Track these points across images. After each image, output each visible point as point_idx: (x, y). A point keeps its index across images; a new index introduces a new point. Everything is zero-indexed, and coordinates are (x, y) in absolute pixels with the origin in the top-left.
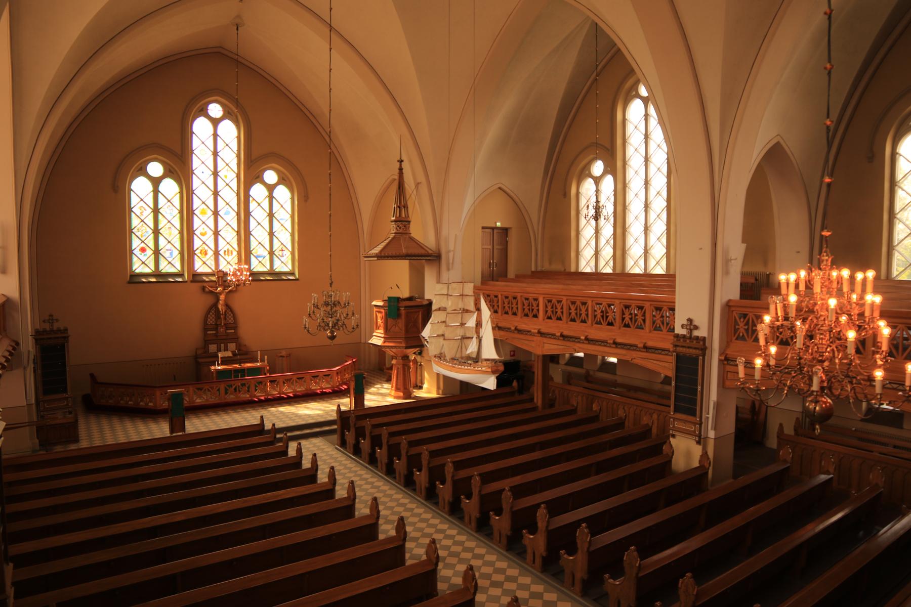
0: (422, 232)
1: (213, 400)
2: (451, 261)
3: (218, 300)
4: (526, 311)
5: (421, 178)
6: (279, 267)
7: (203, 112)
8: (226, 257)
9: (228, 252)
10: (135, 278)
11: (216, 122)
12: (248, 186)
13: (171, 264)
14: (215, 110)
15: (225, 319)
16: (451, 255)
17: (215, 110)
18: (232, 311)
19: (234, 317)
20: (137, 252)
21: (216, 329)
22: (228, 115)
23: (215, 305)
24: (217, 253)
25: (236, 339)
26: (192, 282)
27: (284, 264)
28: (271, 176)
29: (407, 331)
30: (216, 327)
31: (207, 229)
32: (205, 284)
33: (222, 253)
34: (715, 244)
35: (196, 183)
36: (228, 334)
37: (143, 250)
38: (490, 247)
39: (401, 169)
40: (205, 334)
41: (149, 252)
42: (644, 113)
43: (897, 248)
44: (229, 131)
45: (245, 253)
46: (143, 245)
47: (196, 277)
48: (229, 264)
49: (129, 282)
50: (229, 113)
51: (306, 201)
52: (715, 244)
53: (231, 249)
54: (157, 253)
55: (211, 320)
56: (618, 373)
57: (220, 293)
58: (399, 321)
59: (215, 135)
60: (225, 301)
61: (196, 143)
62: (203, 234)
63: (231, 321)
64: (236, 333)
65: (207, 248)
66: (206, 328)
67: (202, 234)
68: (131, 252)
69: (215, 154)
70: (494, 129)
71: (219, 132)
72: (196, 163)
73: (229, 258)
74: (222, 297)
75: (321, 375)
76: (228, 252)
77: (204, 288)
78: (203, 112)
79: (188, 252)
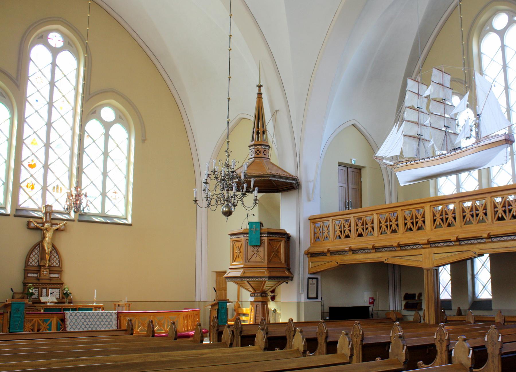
0: (283, 160)
2: (311, 191)
3: (44, 237)
4: (409, 225)
5: (280, 105)
6: (111, 211)
7: (43, 39)
8: (55, 194)
9: (56, 188)
11: (55, 52)
12: (84, 121)
14: (56, 39)
15: (50, 261)
17: (56, 39)
18: (57, 253)
19: (60, 260)
21: (39, 272)
22: (68, 45)
23: (40, 244)
24: (45, 189)
25: (59, 285)
27: (119, 207)
28: (108, 114)
29: (269, 261)
30: (39, 268)
32: (32, 220)
33: (50, 188)
35: (28, 110)
36: (51, 279)
38: (346, 185)
39: (260, 94)
40: (25, 277)
42: (500, 44)
44: (69, 63)
47: (19, 213)
48: (59, 203)
50: (69, 44)
51: (144, 141)
53: (60, 185)
55: (34, 261)
56: (493, 308)
58: (261, 249)
59: (54, 65)
61: (32, 69)
63: (56, 263)
64: (59, 278)
65: (34, 182)
66: (27, 270)
67: (30, 165)
69: (52, 84)
70: (354, 57)
71: (57, 62)
72: (30, 89)
74: (49, 235)
76: (56, 188)
77: (29, 223)
78: (43, 39)
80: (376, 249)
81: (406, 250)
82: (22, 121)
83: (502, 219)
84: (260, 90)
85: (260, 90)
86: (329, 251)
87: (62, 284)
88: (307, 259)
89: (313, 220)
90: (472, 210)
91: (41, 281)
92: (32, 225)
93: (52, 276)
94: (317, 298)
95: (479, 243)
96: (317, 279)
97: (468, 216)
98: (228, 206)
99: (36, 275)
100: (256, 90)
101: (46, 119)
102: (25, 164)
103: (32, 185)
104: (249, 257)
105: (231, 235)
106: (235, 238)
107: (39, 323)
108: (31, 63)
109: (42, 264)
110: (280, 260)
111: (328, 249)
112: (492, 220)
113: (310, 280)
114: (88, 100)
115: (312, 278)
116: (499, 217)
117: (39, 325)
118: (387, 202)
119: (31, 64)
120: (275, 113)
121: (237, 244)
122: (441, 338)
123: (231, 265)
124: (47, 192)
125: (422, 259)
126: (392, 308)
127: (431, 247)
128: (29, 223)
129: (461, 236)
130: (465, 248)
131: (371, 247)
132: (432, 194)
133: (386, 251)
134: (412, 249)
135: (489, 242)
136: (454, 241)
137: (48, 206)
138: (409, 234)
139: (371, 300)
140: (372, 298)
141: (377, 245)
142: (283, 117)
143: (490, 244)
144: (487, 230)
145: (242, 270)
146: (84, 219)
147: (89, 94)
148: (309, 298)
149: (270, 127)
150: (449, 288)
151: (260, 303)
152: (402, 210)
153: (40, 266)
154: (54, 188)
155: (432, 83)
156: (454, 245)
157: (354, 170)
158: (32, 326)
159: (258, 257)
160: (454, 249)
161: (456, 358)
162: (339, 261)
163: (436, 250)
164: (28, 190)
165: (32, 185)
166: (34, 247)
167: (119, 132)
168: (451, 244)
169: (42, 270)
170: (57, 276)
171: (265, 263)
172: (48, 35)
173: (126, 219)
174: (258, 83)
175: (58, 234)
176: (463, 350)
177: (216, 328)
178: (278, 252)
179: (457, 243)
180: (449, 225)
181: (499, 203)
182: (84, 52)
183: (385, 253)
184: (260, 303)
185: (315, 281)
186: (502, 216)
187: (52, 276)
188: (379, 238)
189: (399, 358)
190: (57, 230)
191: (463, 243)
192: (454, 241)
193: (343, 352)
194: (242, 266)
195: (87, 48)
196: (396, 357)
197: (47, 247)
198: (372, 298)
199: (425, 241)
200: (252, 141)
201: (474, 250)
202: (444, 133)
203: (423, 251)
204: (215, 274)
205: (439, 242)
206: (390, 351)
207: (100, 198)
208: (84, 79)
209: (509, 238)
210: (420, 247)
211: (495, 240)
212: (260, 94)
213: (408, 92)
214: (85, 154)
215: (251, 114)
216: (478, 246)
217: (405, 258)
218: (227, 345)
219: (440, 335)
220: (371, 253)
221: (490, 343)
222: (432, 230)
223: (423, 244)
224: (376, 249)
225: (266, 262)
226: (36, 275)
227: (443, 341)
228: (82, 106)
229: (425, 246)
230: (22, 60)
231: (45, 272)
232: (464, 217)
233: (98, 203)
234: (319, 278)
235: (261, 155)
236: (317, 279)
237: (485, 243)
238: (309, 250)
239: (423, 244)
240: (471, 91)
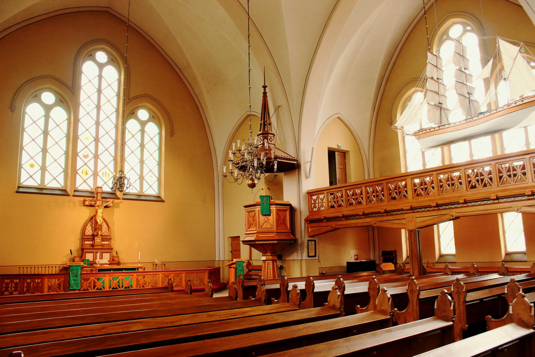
0: (283, 147)
10: (21, 190)
11: (101, 66)
21: (93, 239)
25: (109, 249)
28: (143, 114)
30: (93, 237)
31: (88, 152)
35: (82, 113)
39: (265, 93)
40: (82, 245)
44: (112, 75)
49: (17, 192)
54: (43, 169)
55: (89, 231)
58: (270, 217)
59: (100, 77)
62: (86, 157)
65: (88, 169)
66: (84, 238)
71: (103, 74)
72: (83, 96)
74: (100, 211)
80: (365, 215)
81: (392, 215)
82: (77, 120)
83: (473, 187)
84: (265, 90)
85: (265, 90)
86: (325, 218)
87: (112, 249)
88: (307, 225)
89: (310, 194)
90: (509, 171)
91: (95, 247)
92: (87, 203)
93: (103, 243)
94: (315, 256)
95: (456, 208)
96: (315, 241)
97: (505, 175)
98: (252, 179)
99: (91, 243)
100: (262, 90)
101: (95, 119)
103: (86, 171)
104: (261, 225)
105: (246, 207)
106: (249, 209)
107: (94, 281)
108: (83, 75)
109: (95, 234)
110: (286, 226)
111: (465, 200)
112: (467, 188)
113: (310, 242)
114: (128, 103)
115: (311, 240)
116: (472, 185)
117: (95, 282)
118: (366, 178)
119: (83, 75)
120: (277, 108)
121: (251, 214)
122: (458, 291)
123: (247, 231)
124: (98, 177)
125: (389, 222)
127: (413, 212)
128: (84, 201)
129: (440, 202)
130: (444, 212)
131: (361, 213)
132: (403, 171)
133: (374, 217)
134: (397, 214)
135: (497, 203)
136: (434, 207)
137: (99, 187)
138: (393, 202)
139: (356, 257)
140: (357, 255)
141: (366, 212)
142: (284, 112)
143: (465, 208)
144: (462, 197)
145: (255, 235)
147: (129, 99)
148: (309, 256)
149: (273, 120)
151: (271, 262)
152: (387, 183)
153: (94, 236)
154: (103, 173)
156: (433, 210)
157: (340, 154)
158: (89, 283)
159: (268, 224)
160: (434, 213)
161: (516, 315)
162: (334, 226)
163: (418, 215)
165: (86, 171)
167: (152, 129)
168: (431, 209)
169: (96, 238)
170: (107, 243)
171: (275, 229)
172: (96, 53)
173: (24, 278)
174: (263, 85)
176: (523, 307)
177: (241, 284)
178: (285, 220)
179: (437, 208)
180: (485, 185)
181: (518, 167)
182: (123, 63)
183: (373, 219)
184: (271, 262)
185: (313, 242)
186: (475, 185)
187: (103, 243)
188: (368, 206)
189: (446, 314)
191: (441, 208)
192: (434, 207)
193: (383, 308)
194: (255, 232)
195: (125, 62)
196: (443, 314)
197: (99, 220)
198: (357, 255)
199: (409, 208)
200: (260, 131)
201: (452, 213)
202: (468, 100)
203: (406, 216)
204: (230, 239)
205: (421, 208)
206: (435, 307)
207: (138, 181)
208: (125, 85)
209: (477, 204)
210: (404, 212)
211: (470, 204)
212: (265, 93)
213: (428, 64)
214: (126, 146)
215: (258, 110)
216: (455, 210)
217: (391, 221)
218: (261, 301)
219: (458, 288)
220: (361, 218)
221: (511, 295)
222: (413, 198)
223: (407, 210)
224: (365, 215)
225: (275, 228)
226: (91, 243)
227: (460, 293)
228: (124, 107)
229: (408, 212)
230: (76, 74)
231: (98, 240)
232: (501, 178)
233: (137, 185)
234: (317, 240)
236: (315, 241)
237: (461, 207)
238: (308, 217)
239: (407, 210)
240: (495, 58)
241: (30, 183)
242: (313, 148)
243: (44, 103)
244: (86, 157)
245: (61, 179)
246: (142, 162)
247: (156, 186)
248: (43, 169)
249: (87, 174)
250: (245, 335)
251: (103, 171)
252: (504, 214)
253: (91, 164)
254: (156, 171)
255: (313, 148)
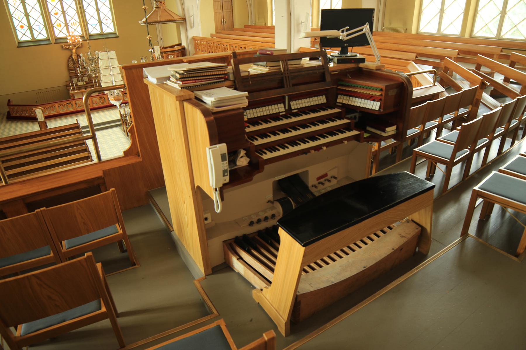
1: (71, 110)
10: (21, 45)
13: (41, 34)
16: (192, 18)
20: (18, 28)
21: (75, 70)
23: (71, 56)
26: (55, 43)
27: (109, 28)
31: (57, 11)
32: (62, 44)
34: (290, 14)
37: (22, 27)
40: (70, 73)
41: (26, 28)
43: (432, 236)
45: (84, 23)
46: (21, 24)
49: (18, 47)
52: (290, 14)
54: (30, 28)
57: (72, 49)
60: (76, 53)
62: (56, 14)
65: (60, 23)
66: (69, 70)
68: (15, 29)
73: (75, 27)
74: (74, 51)
75: (453, 58)
77: (62, 47)
79: (49, 26)
102: (52, 13)
126: (266, 339)
146: (91, 37)
150: (319, 98)
155: (481, 104)
164: (58, 28)
166: (69, 58)
175: (79, 49)
190: (78, 47)
207: (98, 25)
235: (159, 6)
241: (25, 39)
242: (294, 85)
243: (247, 107)
244: (56, 14)
245: (44, 32)
246: (98, 10)
247: (112, 26)
248: (30, 28)
249: (60, 26)
250: (266, 276)
251: (71, 22)
252: (119, 311)
253: (62, 18)
254: (109, 15)
255: (294, 85)
